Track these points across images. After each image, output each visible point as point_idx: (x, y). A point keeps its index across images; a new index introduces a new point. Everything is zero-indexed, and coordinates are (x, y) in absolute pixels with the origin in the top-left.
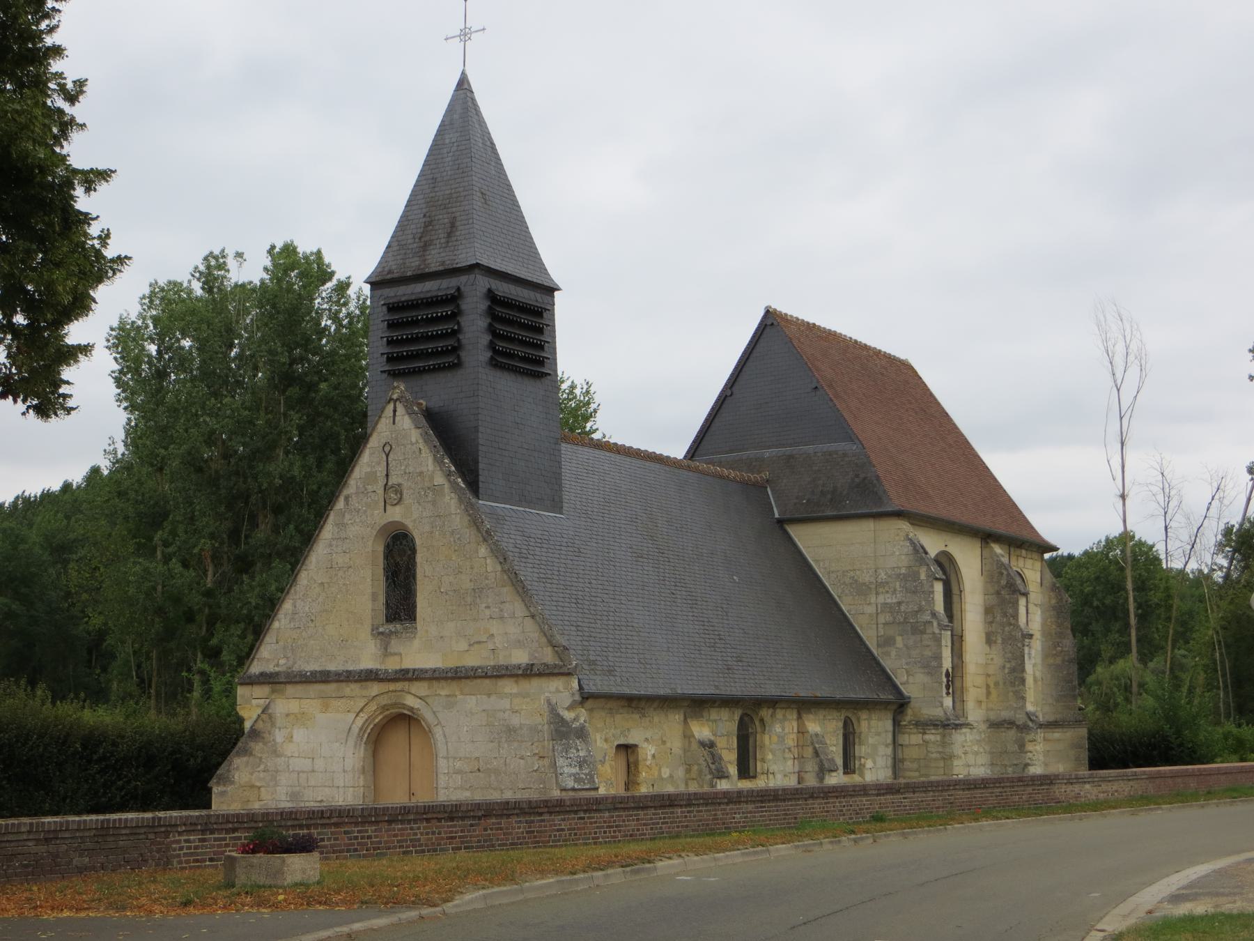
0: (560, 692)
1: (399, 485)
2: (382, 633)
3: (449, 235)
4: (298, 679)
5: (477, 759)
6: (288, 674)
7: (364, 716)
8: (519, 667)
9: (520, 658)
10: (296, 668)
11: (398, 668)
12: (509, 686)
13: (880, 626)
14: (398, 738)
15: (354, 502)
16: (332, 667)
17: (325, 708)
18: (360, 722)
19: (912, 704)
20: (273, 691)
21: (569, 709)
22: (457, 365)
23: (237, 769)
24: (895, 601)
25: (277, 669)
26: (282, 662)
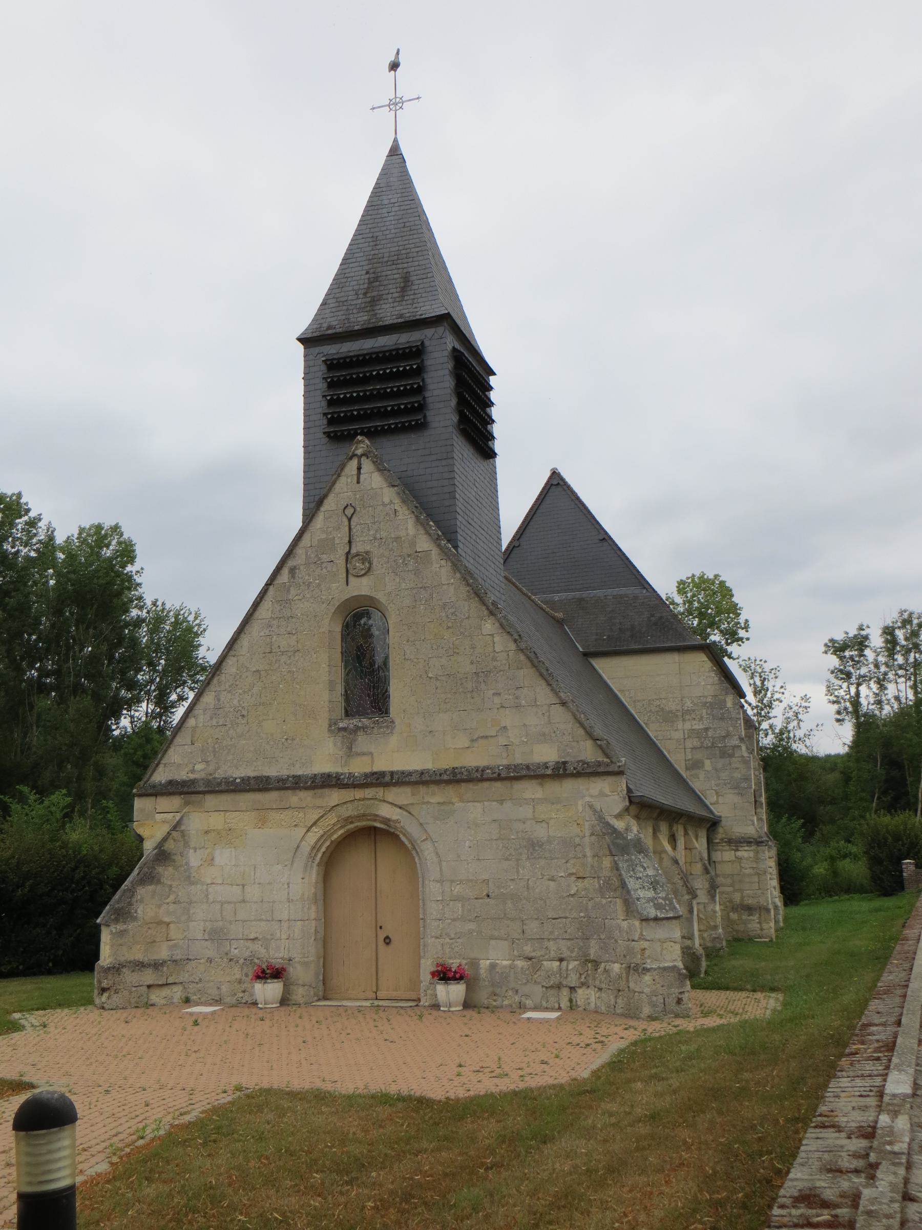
0: (607, 796)
1: (367, 553)
2: (344, 729)
3: (403, 290)
4: (223, 787)
5: (486, 882)
6: (208, 782)
7: (317, 832)
8: (546, 766)
9: (547, 754)
10: (220, 774)
11: (368, 770)
12: (530, 790)
13: (688, 750)
14: (357, 862)
15: (302, 573)
16: (272, 771)
17: (262, 822)
18: (312, 838)
19: (723, 823)
20: (187, 803)
21: (619, 816)
22: (420, 426)
23: (141, 901)
24: (702, 727)
25: (192, 776)
26: (198, 767)
